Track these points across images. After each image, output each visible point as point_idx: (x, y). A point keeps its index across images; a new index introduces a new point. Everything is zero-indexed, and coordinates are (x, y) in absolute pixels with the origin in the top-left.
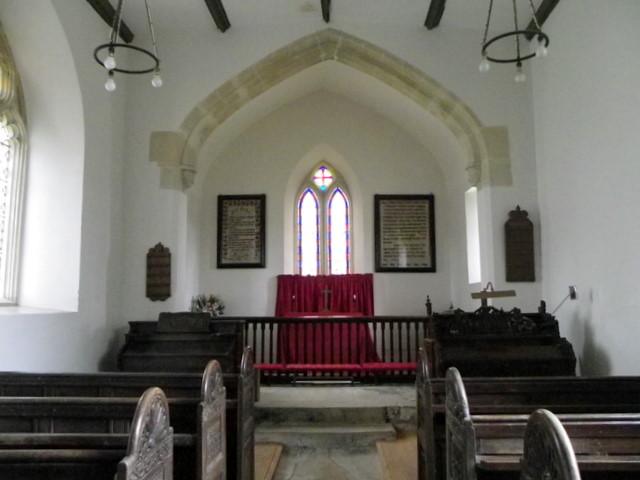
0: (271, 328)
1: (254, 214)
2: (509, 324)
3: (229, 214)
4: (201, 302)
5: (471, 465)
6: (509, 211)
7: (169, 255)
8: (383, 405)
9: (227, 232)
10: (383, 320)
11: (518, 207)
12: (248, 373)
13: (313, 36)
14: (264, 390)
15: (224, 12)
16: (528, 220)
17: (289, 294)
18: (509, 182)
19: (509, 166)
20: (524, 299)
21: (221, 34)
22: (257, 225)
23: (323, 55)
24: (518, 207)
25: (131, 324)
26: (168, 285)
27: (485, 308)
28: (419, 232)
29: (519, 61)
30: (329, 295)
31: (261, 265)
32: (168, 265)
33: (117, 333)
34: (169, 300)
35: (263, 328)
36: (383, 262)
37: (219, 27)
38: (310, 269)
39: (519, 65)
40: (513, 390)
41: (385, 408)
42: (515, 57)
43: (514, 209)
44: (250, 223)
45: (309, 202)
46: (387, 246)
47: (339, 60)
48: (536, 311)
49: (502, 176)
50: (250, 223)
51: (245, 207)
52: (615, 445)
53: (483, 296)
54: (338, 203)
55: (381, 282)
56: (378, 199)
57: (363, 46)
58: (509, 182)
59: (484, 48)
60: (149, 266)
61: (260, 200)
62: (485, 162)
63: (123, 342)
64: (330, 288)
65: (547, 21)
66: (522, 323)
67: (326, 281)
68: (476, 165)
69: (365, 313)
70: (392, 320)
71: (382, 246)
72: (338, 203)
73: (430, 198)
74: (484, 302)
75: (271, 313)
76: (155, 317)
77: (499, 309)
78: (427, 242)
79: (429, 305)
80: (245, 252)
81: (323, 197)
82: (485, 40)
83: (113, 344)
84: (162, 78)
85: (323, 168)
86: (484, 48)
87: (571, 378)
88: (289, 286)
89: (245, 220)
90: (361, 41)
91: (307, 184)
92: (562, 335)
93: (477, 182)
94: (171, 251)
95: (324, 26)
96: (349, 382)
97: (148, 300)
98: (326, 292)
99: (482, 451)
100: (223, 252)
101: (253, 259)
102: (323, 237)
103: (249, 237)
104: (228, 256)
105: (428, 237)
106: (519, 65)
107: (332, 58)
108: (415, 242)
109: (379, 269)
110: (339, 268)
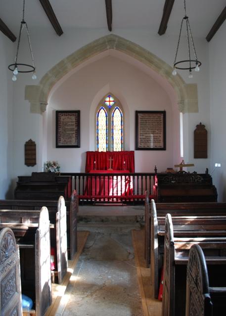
0: (83, 178)
1: (74, 120)
2: (191, 178)
3: (62, 120)
4: (49, 165)
5: (155, 234)
6: (196, 125)
7: (35, 145)
8: (135, 215)
9: (60, 130)
10: (138, 175)
11: (201, 123)
12: (74, 201)
13: (103, 38)
14: (81, 208)
15: (61, 30)
16: (205, 129)
17: (92, 162)
18: (197, 111)
19: (197, 103)
20: (199, 166)
21: (59, 37)
22: (76, 126)
23: (108, 47)
24: (201, 123)
25: (19, 177)
26: (35, 159)
27: (181, 171)
28: (158, 130)
29: (190, 69)
30: (112, 161)
31: (78, 146)
32: (35, 150)
33: (12, 181)
34: (35, 166)
35: (79, 178)
36: (139, 145)
37: (57, 34)
38: (102, 148)
39: (190, 71)
40: (183, 208)
41: (136, 216)
42: (189, 67)
43: (199, 124)
44: (72, 125)
45: (102, 115)
46: (142, 137)
47: (116, 49)
48: (205, 173)
49: (194, 108)
50: (72, 125)
51: (70, 117)
52: (208, 227)
53: (182, 165)
54: (117, 115)
55: (138, 155)
56: (137, 113)
57: (128, 43)
58: (197, 111)
59: (175, 65)
60: (26, 150)
61: (77, 113)
62: (186, 101)
63: (16, 185)
64: (112, 158)
65: (212, 40)
66: (197, 178)
67: (110, 154)
68: (182, 102)
69: (131, 171)
70: (142, 175)
71: (139, 137)
72: (117, 115)
73: (164, 113)
74: (181, 169)
75: (84, 172)
76: (30, 174)
77: (188, 172)
78: (162, 135)
79: (156, 170)
80: (70, 140)
81: (109, 110)
82: (175, 61)
83: (11, 187)
84: (36, 75)
85: (109, 96)
86: (175, 65)
87: (215, 203)
88: (92, 157)
89: (70, 123)
90: (128, 41)
91: (102, 104)
92: (213, 184)
93: (183, 111)
94: (36, 143)
95: (108, 33)
96: (121, 204)
97: (26, 166)
98: (111, 160)
99: (161, 229)
100: (59, 139)
101: (73, 144)
102: (109, 132)
103: (72, 132)
104: (61, 142)
105: (162, 132)
106: (190, 71)
107: (113, 48)
108: (156, 135)
109: (137, 148)
110: (117, 147)
